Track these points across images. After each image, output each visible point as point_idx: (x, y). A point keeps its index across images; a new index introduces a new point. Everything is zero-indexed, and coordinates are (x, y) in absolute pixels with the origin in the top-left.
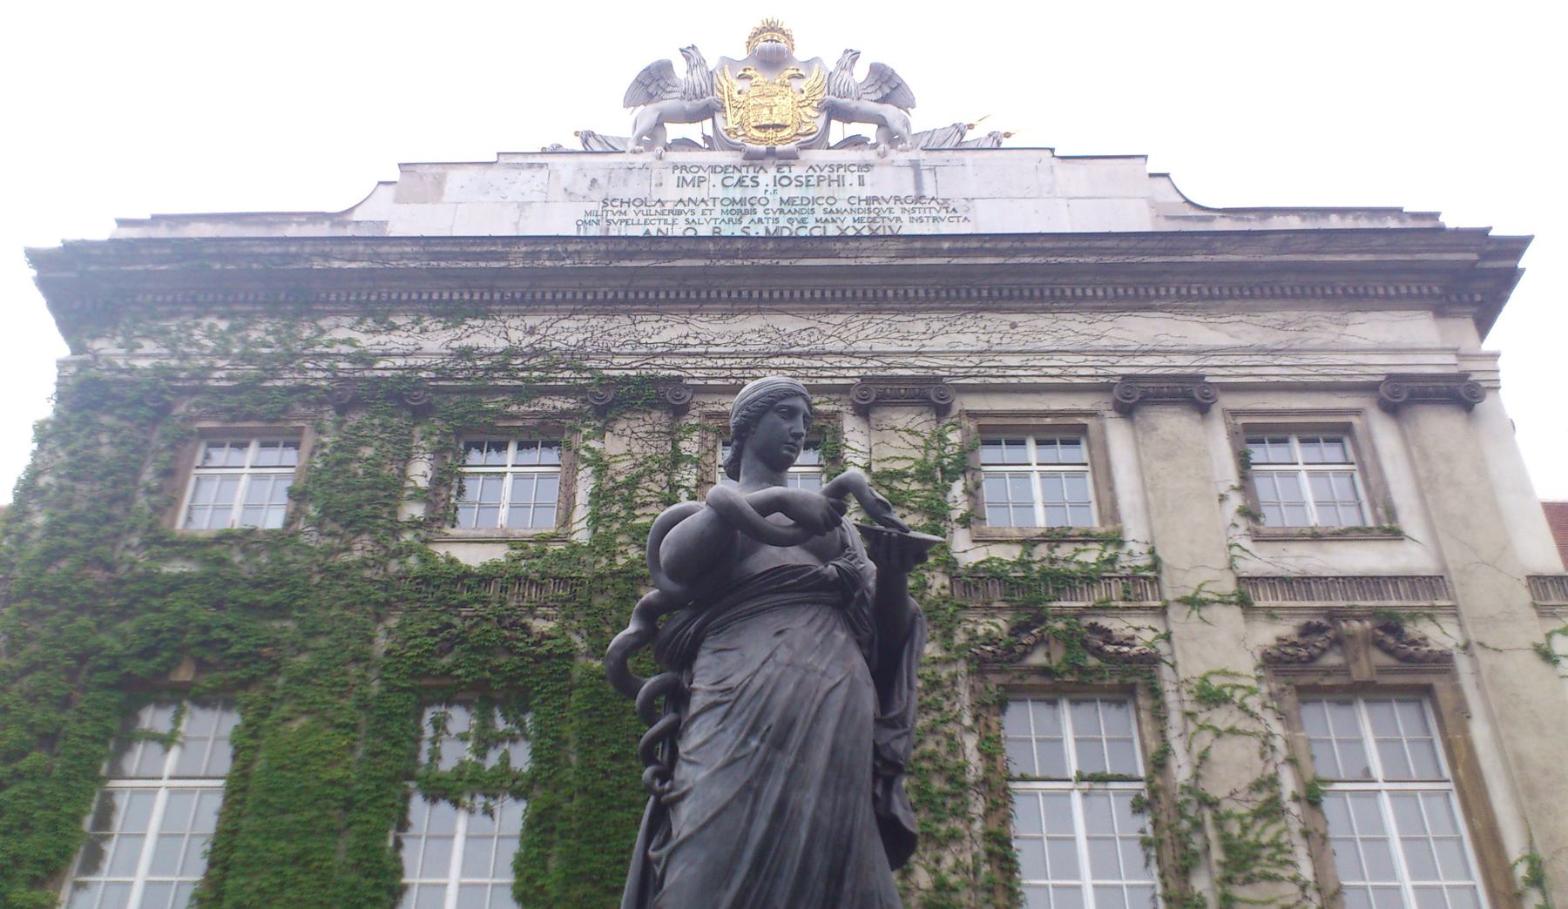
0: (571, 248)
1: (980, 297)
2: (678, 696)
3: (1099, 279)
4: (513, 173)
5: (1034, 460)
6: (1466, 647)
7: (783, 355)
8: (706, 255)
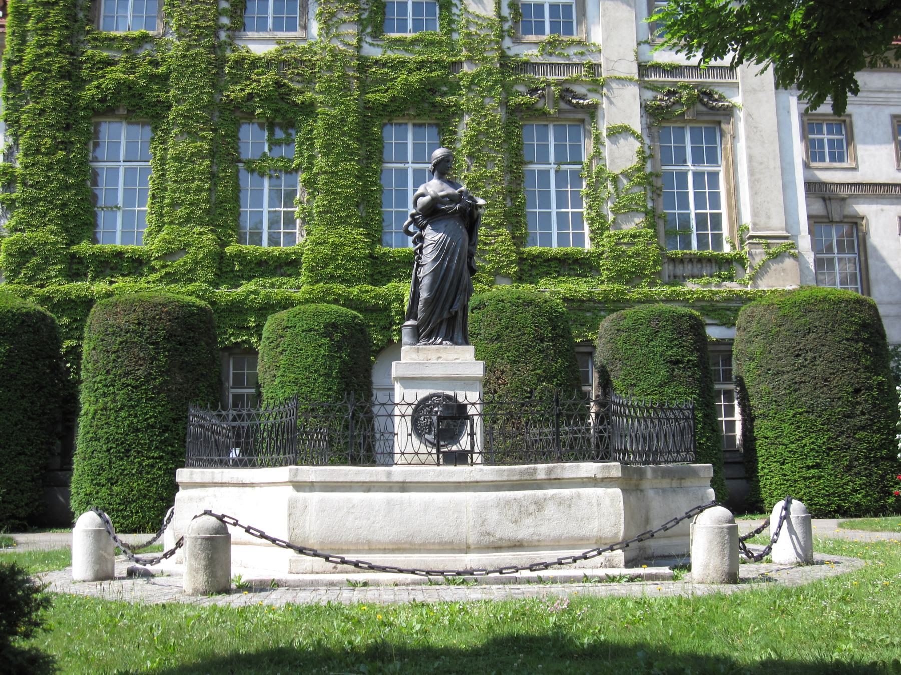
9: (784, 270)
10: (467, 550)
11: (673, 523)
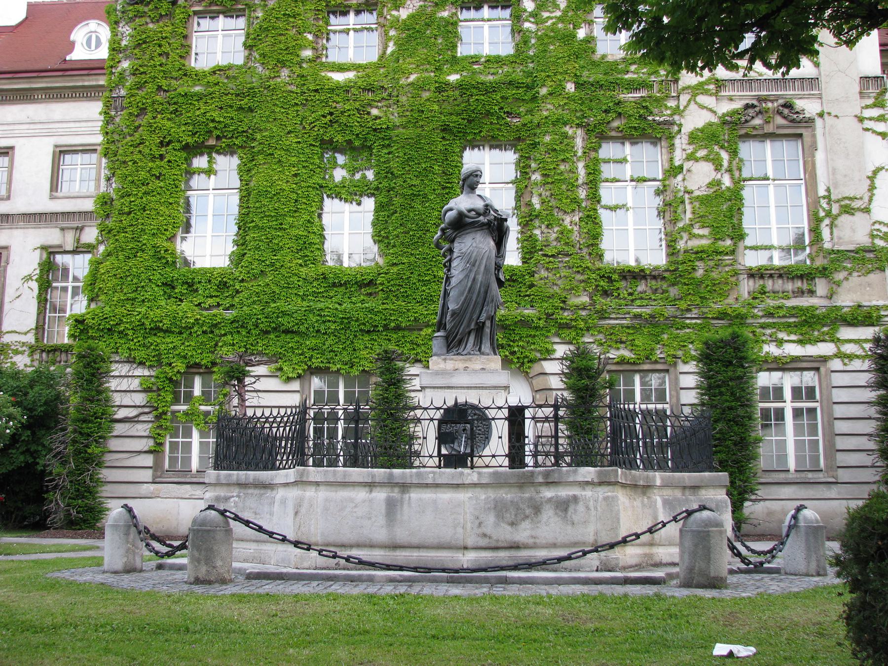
2: (451, 251)
6: (821, 115)
9: (869, 285)
10: (372, 546)
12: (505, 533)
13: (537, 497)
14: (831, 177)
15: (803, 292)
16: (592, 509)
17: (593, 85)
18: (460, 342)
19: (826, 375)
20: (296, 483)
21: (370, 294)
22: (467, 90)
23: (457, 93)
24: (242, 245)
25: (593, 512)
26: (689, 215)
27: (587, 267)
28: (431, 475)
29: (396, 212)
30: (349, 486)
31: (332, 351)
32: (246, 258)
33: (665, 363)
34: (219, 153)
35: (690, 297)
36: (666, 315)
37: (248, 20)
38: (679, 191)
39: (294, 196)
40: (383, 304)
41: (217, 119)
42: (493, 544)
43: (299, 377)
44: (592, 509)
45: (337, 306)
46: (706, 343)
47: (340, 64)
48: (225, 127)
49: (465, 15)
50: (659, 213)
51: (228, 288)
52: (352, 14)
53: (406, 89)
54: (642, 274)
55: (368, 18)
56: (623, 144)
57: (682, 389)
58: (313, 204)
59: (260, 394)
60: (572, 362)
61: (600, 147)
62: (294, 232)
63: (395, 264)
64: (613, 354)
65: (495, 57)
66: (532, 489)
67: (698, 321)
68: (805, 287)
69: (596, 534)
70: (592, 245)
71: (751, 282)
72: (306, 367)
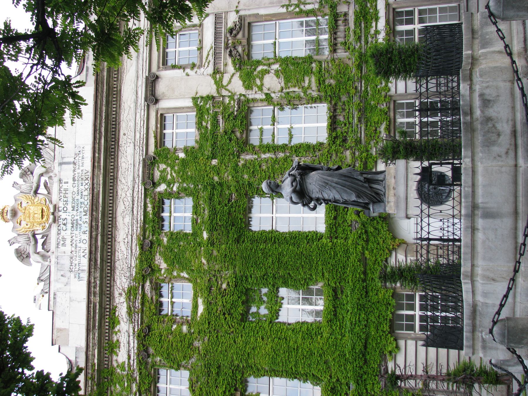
0: (93, 281)
1: (114, 145)
3: (110, 106)
4: (57, 304)
5: (171, 131)
6: (237, 12)
7: (133, 210)
8: (97, 235)
10: (516, 229)
11: (501, 36)
12: (505, 140)
13: (480, 120)
14: (275, 5)
15: (346, 20)
16: (488, 84)
17: (214, 148)
18: (377, 194)
19: (398, 4)
20: (473, 282)
21: (342, 292)
22: (213, 226)
23: (215, 233)
24: (307, 376)
25: (491, 83)
26: (296, 89)
27: (328, 151)
28: (466, 189)
29: (289, 274)
30: (474, 244)
31: (379, 317)
32: (315, 374)
33: (389, 103)
34: (246, 390)
35: (347, 88)
36: (359, 102)
37: (161, 367)
38: (281, 95)
39: (276, 340)
40: (348, 282)
41: (224, 389)
42: (513, 147)
43: (396, 340)
44: (488, 84)
45: (349, 313)
46: (377, 74)
47: (193, 308)
48: (229, 384)
49: (166, 229)
50: (294, 108)
51: (335, 387)
52: (162, 299)
53: (211, 265)
54: (332, 117)
55: (165, 289)
56: (251, 130)
57: (406, 92)
58: (282, 327)
59: (407, 365)
60: (388, 159)
61: (252, 144)
62: (300, 340)
63: (323, 274)
64: (383, 135)
65: (193, 209)
66: (475, 123)
67: (363, 82)
68: (342, 18)
69: (505, 81)
70: (314, 149)
71: (339, 51)
72: (389, 335)
